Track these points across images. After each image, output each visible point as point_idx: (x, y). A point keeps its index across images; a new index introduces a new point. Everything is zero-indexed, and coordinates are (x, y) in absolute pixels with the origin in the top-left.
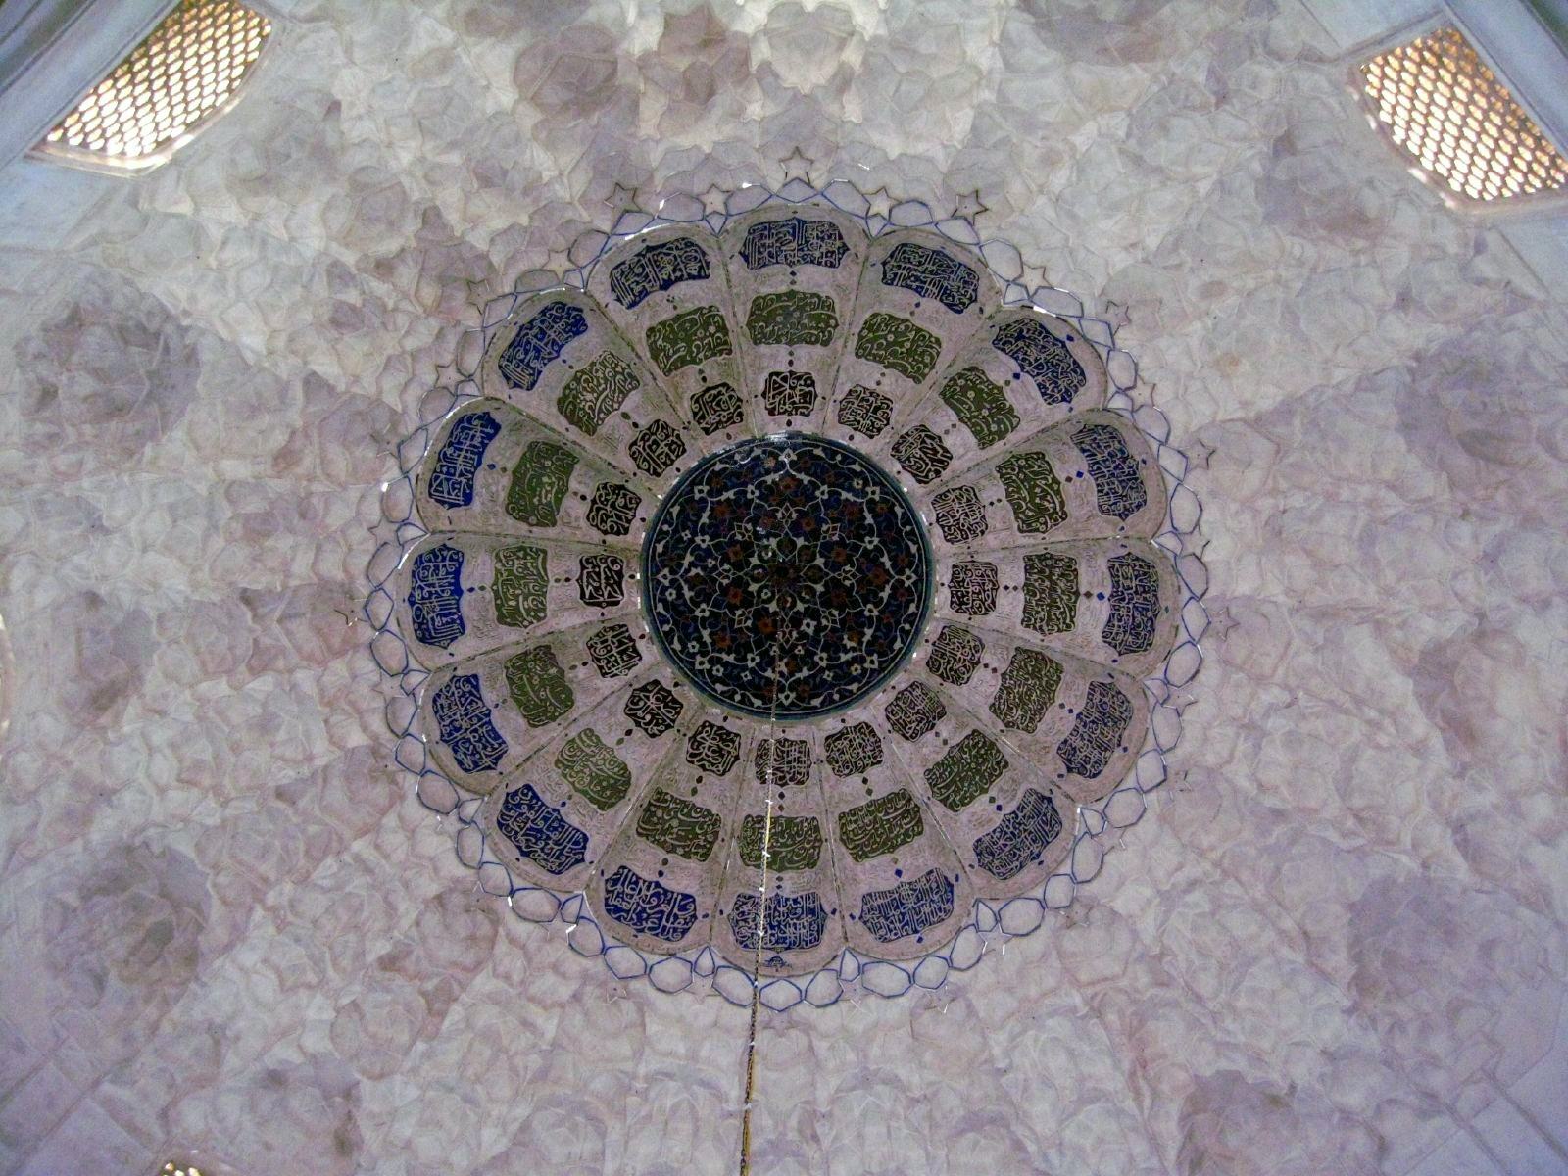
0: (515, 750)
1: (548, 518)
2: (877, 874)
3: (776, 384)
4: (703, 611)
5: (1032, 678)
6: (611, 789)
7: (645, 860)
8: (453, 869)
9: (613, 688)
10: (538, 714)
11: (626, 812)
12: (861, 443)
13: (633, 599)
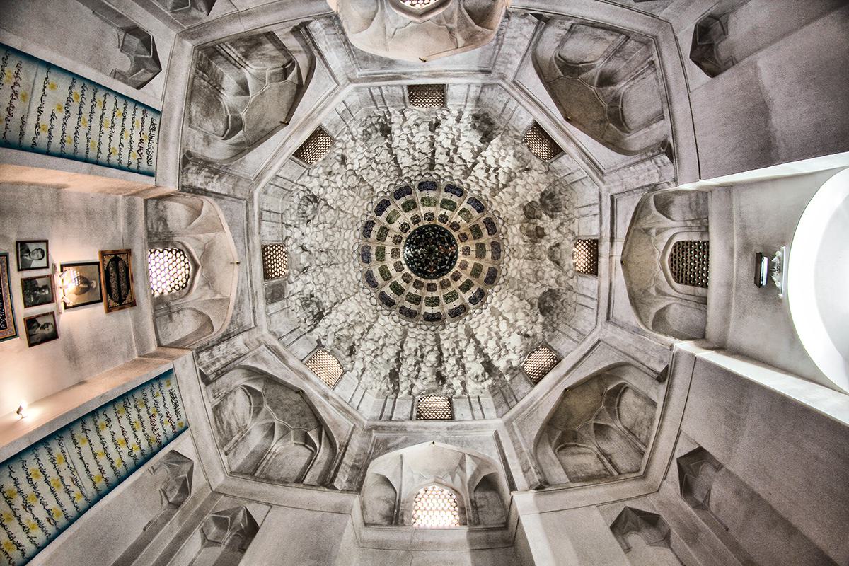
0: (397, 202)
1: (442, 207)
2: (376, 273)
3: (468, 248)
4: (423, 236)
5: (417, 300)
6: (389, 221)
7: (376, 228)
8: (378, 190)
9: (409, 220)
10: (404, 206)
11: (386, 223)
12: (457, 265)
13: (427, 223)
